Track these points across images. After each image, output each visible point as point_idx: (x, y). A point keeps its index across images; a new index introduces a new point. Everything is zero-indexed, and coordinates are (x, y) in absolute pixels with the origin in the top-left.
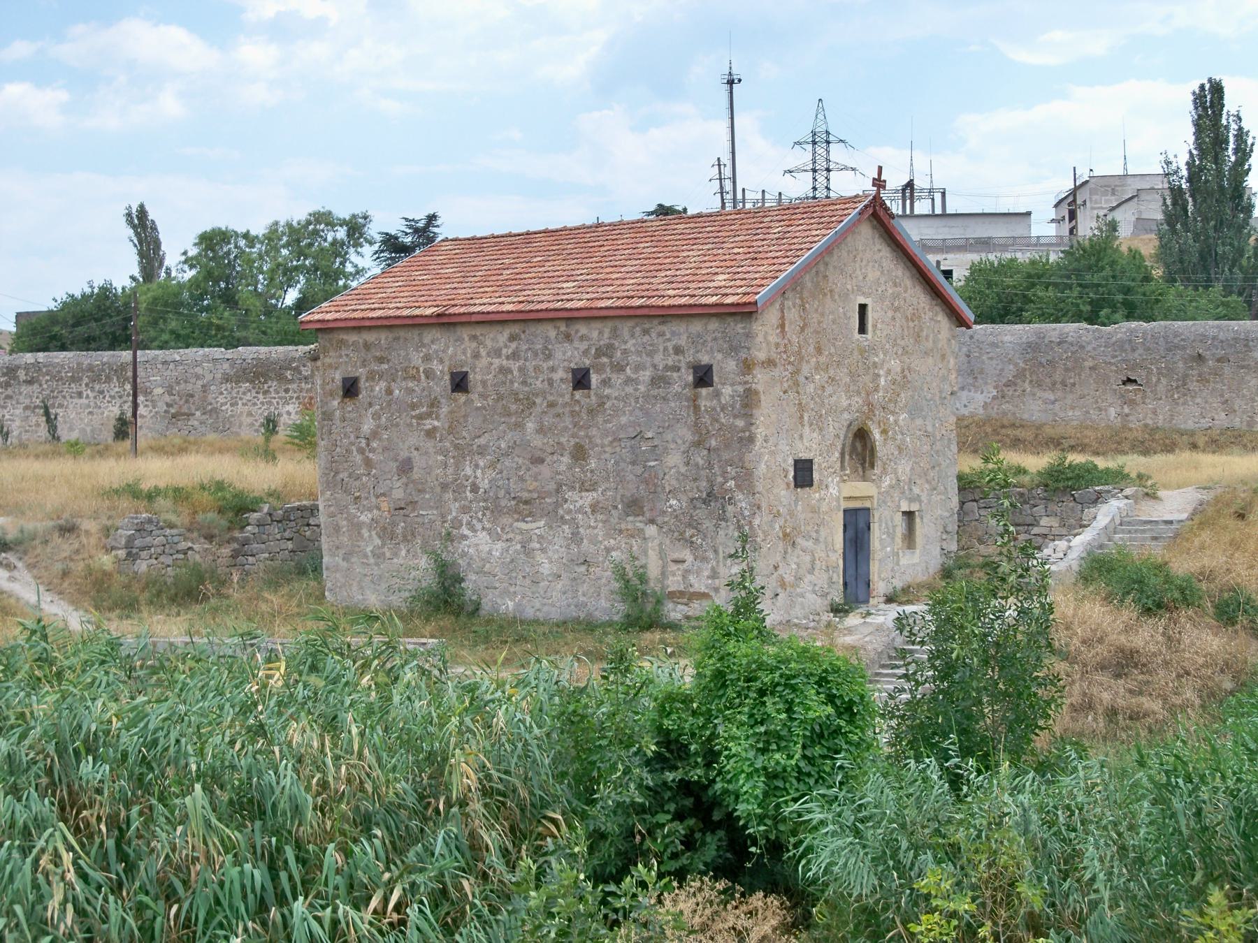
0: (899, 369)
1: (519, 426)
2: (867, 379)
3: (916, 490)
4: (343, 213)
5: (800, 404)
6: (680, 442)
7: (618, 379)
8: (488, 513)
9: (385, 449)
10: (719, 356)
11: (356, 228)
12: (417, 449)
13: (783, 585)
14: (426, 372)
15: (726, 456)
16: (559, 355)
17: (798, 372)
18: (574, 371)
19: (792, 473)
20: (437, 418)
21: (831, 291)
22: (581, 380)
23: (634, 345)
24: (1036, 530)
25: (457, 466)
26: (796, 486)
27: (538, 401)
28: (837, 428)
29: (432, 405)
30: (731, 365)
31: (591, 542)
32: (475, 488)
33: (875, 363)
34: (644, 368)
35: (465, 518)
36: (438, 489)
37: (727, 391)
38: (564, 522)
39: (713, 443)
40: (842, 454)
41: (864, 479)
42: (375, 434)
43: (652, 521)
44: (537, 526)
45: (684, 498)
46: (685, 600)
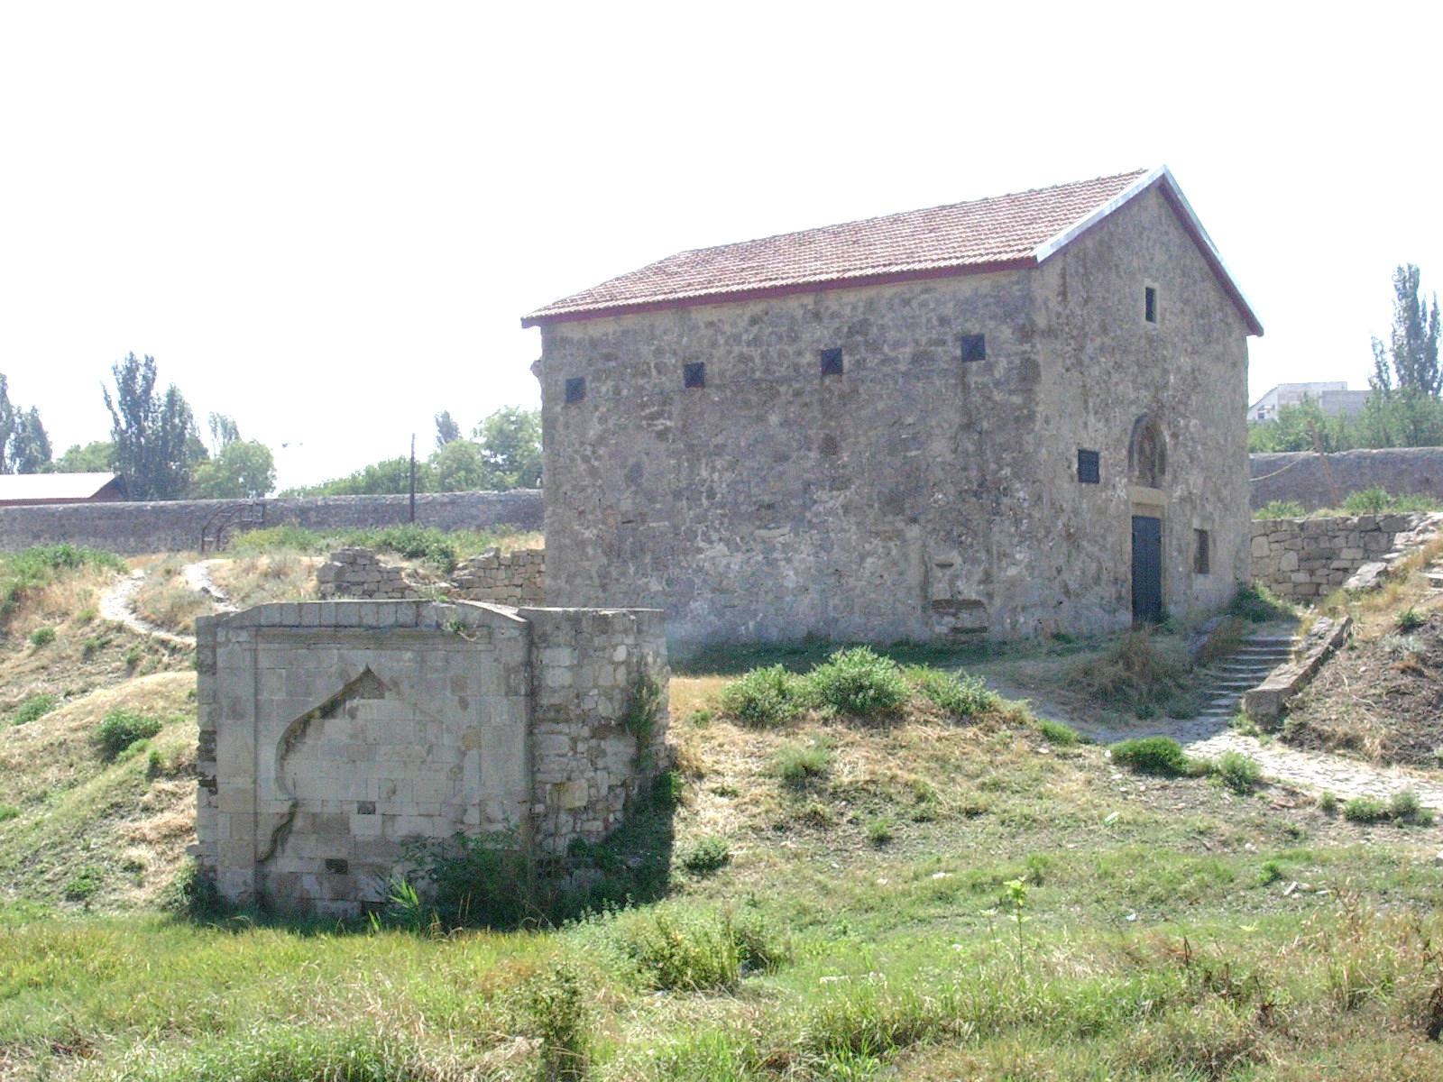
0: (1189, 369)
1: (761, 419)
2: (1156, 373)
3: (1209, 508)
5: (1084, 386)
6: (946, 426)
7: (873, 361)
8: (726, 520)
9: (612, 456)
10: (991, 324)
12: (647, 454)
13: (1067, 592)
14: (656, 366)
15: (1000, 439)
16: (806, 336)
17: (1081, 349)
18: (823, 353)
19: (1075, 466)
20: (670, 418)
21: (1117, 266)
22: (831, 363)
23: (892, 319)
24: (1336, 564)
25: (691, 468)
26: (1081, 480)
27: (783, 389)
28: (1123, 419)
29: (664, 403)
30: (1006, 332)
31: (843, 549)
32: (711, 495)
33: (1164, 356)
34: (905, 345)
35: (701, 528)
36: (670, 498)
38: (811, 525)
39: (985, 425)
40: (1130, 452)
41: (1153, 485)
42: (601, 440)
43: (914, 520)
45: (952, 490)
46: (952, 610)
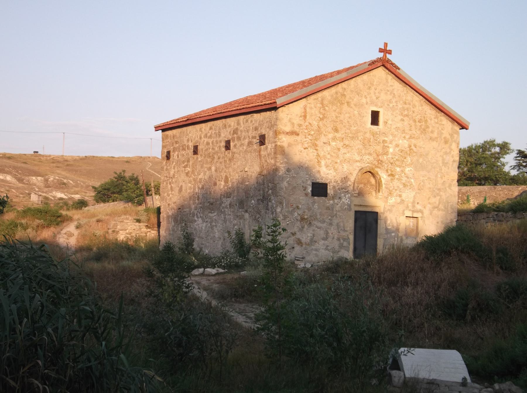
4: (499, 141)
11: (504, 148)
37: (269, 147)
43: (246, 211)
44: (214, 215)
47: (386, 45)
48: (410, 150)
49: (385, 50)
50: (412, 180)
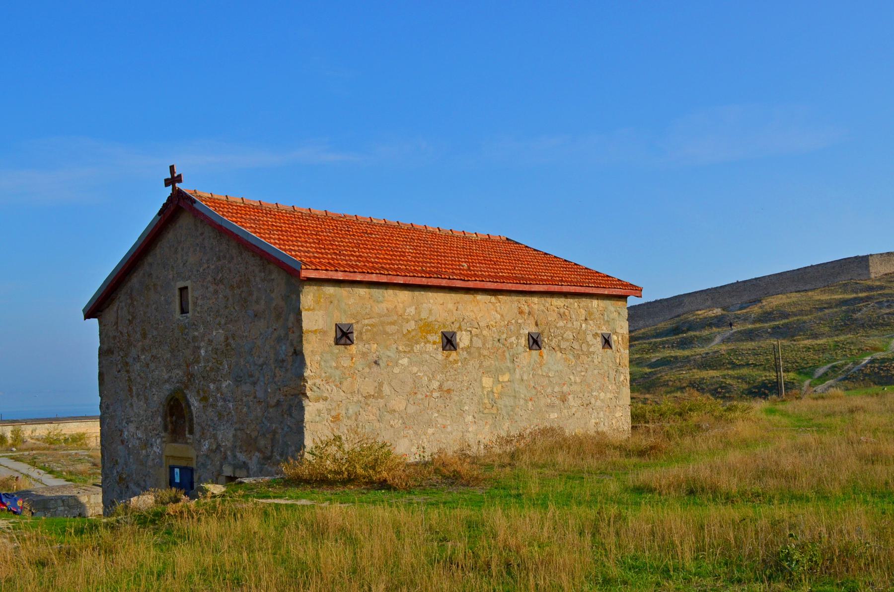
47: (172, 168)
48: (227, 345)
49: (173, 180)
50: (231, 405)
